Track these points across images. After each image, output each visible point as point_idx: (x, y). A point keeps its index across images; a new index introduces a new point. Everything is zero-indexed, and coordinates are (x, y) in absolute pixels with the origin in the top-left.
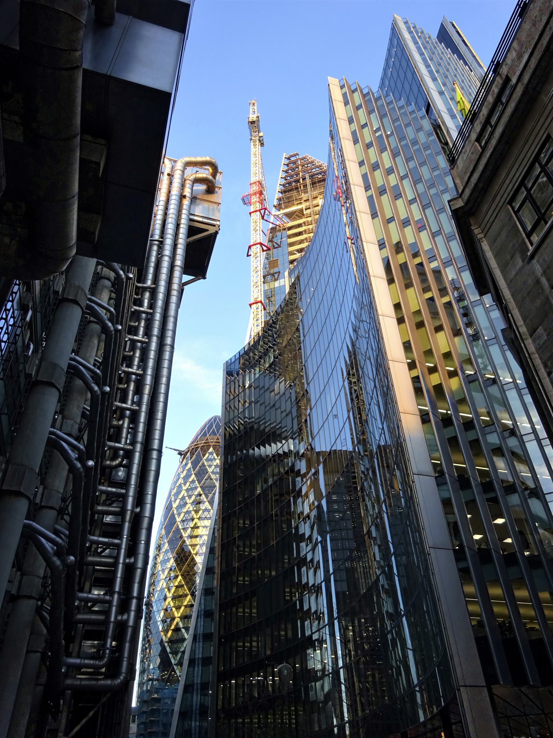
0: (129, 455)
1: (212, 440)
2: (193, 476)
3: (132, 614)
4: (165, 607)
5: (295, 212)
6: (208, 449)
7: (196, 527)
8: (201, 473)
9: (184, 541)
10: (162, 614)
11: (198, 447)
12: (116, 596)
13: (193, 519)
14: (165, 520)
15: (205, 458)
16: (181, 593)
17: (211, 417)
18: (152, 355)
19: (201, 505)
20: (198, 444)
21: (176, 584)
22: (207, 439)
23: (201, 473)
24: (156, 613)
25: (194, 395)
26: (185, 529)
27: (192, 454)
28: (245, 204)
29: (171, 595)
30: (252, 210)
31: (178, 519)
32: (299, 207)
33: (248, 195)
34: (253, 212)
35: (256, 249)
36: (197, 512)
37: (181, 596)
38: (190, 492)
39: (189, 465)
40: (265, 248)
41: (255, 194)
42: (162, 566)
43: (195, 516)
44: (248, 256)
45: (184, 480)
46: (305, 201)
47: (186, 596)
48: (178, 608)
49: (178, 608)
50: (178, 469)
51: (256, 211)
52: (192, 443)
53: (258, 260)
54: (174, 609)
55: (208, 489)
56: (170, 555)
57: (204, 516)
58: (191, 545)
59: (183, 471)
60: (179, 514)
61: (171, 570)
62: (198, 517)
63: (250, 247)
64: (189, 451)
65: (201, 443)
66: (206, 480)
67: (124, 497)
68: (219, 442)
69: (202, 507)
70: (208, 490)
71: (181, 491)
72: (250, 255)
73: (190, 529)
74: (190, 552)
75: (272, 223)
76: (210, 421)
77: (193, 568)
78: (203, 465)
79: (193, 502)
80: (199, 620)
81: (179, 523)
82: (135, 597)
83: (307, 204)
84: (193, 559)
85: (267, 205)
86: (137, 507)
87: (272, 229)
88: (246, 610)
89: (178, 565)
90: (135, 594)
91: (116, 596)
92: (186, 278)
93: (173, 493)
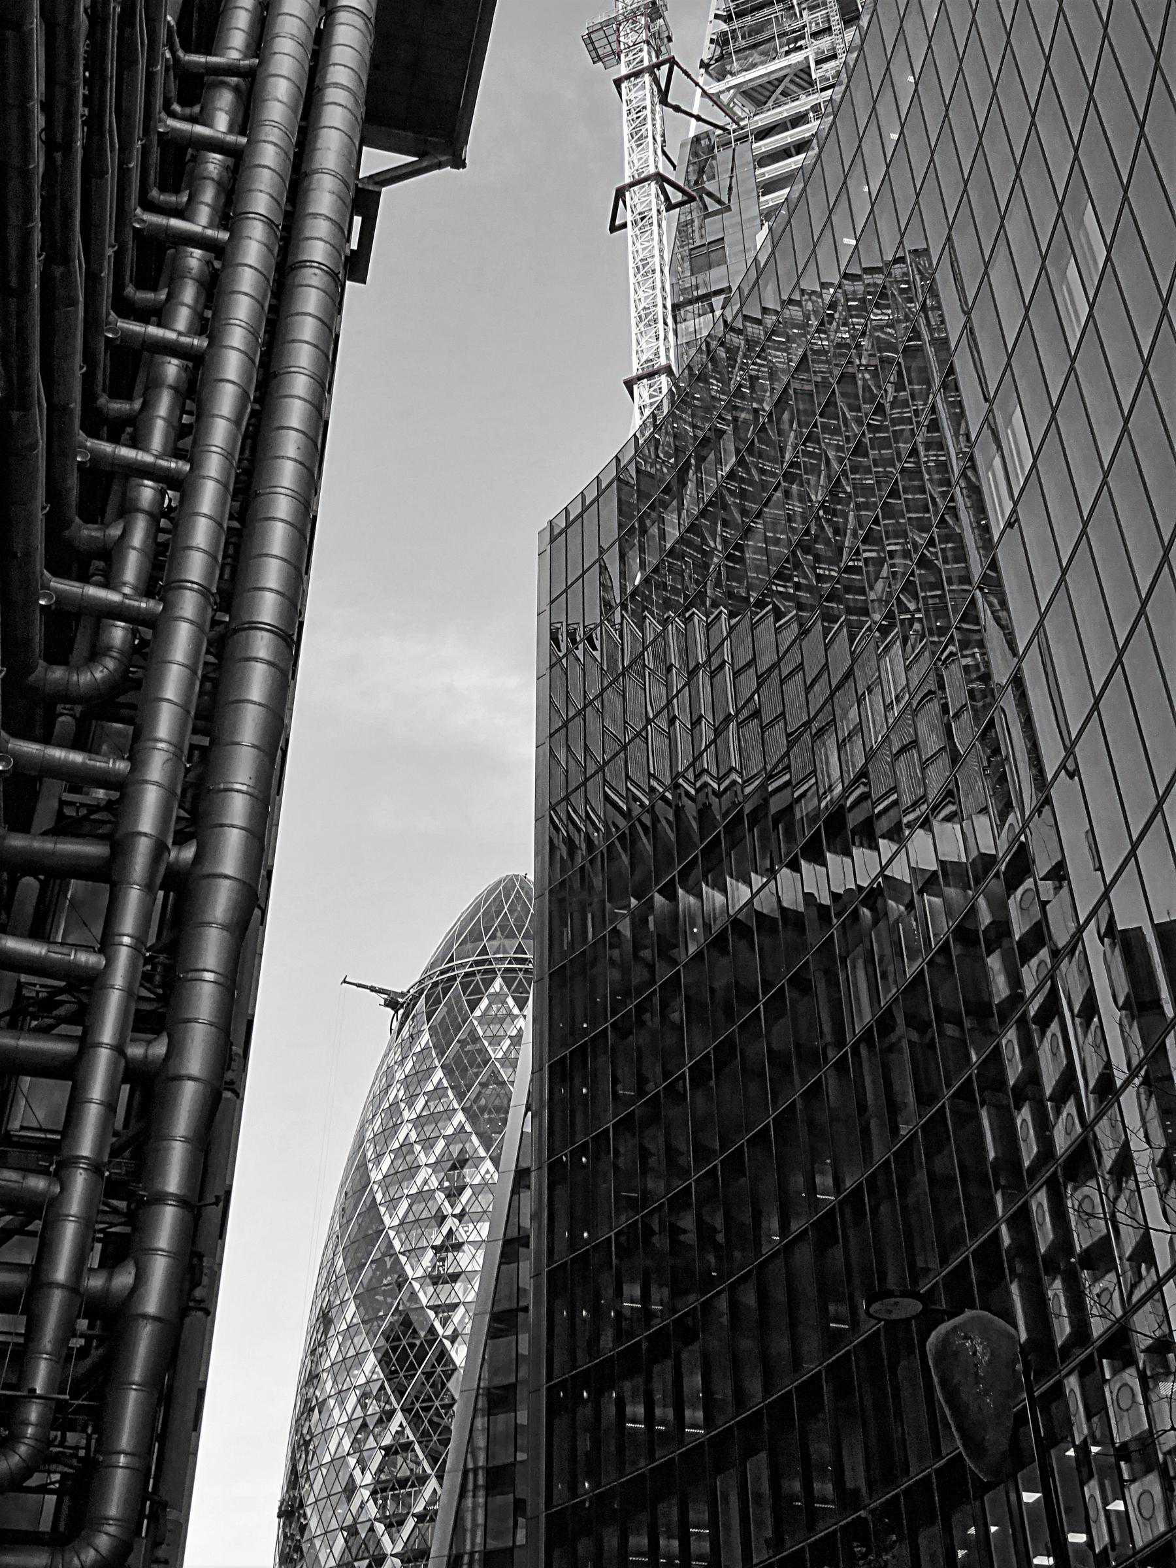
0: (149, 636)
1: (501, 951)
2: (439, 1074)
3: (159, 1268)
4: (349, 1521)
5: (780, 80)
6: (489, 983)
7: (451, 1245)
8: (467, 1065)
9: (413, 1296)
10: (340, 1543)
11: (454, 978)
12: (80, 1180)
13: (441, 1219)
14: (344, 1226)
15: (478, 1013)
16: (404, 1473)
17: (493, 881)
18: (226, 400)
19: (466, 1171)
20: (452, 969)
21: (387, 1440)
22: (484, 951)
23: (467, 1065)
24: (317, 1543)
25: (405, 770)
26: (414, 1253)
27: (433, 1003)
28: (598, 58)
29: (368, 1479)
30: (624, 70)
31: (376, 1176)
32: (796, 58)
33: (608, 23)
34: (628, 77)
35: (647, 198)
36: (453, 1194)
37: (403, 1483)
38: (428, 1129)
39: (425, 1038)
40: (676, 197)
41: (632, 17)
42: (335, 1381)
43: (447, 1209)
44: (613, 228)
45: (407, 1088)
46: (815, 35)
47: (423, 1480)
48: (394, 1524)
49: (394, 1524)
50: (386, 1055)
51: (637, 74)
52: (433, 965)
53: (652, 242)
54: (380, 1527)
55: (488, 1117)
56: (362, 1341)
57: (477, 1208)
58: (436, 1309)
59: (404, 1058)
60: (393, 1203)
61: (365, 1395)
62: (457, 1211)
63: (620, 194)
64: (421, 992)
65: (463, 966)
66: (483, 1085)
67: (124, 790)
68: (524, 961)
69: (473, 1177)
70: (490, 1121)
71: (396, 1127)
72: (624, 226)
73: (430, 1253)
74: (432, 1330)
75: (698, 118)
76: (490, 892)
77: (444, 1385)
78: (474, 1038)
79: (438, 1162)
80: (469, 1502)
81: (392, 1234)
82: (172, 1194)
83: (824, 43)
84: (443, 1354)
85: (675, 50)
86: (181, 839)
87: (697, 139)
88: (658, 1412)
89: (391, 1376)
90: (173, 1181)
91: (80, 1180)
92: (375, 161)
93: (369, 1135)
